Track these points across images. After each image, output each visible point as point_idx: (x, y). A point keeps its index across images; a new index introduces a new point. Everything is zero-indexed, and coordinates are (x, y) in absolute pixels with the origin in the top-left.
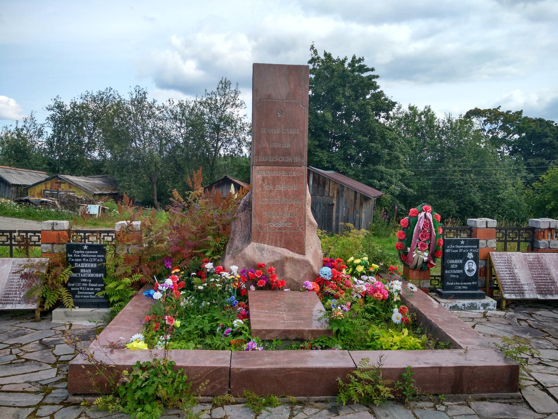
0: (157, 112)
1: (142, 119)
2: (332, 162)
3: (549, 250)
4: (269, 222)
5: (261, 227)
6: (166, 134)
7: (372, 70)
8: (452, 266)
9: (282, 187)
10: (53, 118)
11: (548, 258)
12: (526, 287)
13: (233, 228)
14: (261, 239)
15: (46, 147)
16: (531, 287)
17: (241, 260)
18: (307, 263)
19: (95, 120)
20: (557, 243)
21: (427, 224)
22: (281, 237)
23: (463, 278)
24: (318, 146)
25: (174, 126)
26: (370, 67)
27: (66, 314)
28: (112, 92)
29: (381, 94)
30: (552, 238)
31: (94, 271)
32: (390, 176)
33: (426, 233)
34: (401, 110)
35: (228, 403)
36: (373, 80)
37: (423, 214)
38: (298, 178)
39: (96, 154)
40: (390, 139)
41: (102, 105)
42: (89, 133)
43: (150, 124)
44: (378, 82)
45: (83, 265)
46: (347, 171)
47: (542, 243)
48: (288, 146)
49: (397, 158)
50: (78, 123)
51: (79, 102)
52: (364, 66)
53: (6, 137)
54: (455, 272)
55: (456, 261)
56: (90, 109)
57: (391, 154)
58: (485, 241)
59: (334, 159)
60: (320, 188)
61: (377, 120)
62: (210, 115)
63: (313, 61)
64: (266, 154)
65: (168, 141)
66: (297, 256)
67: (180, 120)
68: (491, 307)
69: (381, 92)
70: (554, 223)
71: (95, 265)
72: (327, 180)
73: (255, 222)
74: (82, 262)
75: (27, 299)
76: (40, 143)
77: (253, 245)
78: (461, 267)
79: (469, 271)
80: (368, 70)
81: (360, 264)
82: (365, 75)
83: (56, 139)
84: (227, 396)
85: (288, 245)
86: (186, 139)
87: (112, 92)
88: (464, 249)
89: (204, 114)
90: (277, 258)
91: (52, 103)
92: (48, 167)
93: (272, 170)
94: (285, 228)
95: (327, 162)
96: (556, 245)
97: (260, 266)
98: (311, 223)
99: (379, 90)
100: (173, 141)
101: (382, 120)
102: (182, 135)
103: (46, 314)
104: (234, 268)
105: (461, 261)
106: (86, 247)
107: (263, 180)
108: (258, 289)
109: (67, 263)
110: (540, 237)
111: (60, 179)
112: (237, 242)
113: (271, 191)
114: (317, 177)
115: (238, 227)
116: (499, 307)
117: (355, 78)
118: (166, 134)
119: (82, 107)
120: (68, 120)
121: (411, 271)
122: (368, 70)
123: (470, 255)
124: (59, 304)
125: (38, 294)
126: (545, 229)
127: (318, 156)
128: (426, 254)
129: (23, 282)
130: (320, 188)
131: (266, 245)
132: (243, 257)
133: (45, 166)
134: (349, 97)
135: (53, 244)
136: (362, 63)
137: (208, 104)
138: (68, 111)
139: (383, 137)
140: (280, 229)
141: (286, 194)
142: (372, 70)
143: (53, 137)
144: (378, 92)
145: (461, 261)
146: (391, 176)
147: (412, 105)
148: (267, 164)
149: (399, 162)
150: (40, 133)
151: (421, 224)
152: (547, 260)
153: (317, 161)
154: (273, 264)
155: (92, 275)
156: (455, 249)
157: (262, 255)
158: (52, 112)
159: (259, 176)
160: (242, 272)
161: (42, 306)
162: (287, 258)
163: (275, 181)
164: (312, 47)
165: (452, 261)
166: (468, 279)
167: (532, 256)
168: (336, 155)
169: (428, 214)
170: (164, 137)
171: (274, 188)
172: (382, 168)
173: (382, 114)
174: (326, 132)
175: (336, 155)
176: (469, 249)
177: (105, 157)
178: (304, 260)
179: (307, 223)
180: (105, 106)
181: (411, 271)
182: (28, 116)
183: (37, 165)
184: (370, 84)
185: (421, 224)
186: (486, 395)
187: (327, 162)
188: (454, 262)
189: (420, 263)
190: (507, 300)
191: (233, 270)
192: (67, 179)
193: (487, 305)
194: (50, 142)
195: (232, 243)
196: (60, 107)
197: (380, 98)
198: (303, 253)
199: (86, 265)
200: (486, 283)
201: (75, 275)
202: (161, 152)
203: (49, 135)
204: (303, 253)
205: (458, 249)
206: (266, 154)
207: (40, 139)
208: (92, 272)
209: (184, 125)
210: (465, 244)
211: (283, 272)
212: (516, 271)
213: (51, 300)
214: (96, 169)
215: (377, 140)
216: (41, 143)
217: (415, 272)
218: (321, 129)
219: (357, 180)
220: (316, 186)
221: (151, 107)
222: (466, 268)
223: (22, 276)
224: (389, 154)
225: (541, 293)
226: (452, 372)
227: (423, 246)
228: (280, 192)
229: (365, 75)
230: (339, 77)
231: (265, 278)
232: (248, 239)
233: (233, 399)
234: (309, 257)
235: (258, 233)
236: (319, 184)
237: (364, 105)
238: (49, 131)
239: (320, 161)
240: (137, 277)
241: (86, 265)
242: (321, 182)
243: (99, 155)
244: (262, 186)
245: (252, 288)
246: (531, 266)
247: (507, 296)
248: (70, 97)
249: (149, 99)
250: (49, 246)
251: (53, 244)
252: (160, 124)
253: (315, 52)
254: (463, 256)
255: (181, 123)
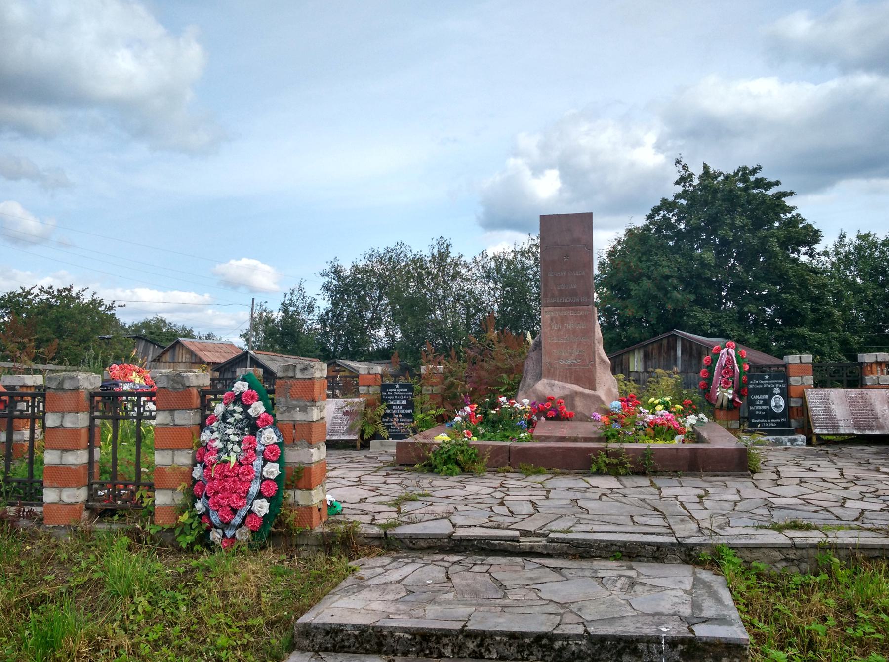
0: (463, 271)
1: (444, 281)
2: (720, 326)
3: (877, 385)
4: (559, 359)
5: (551, 364)
6: (476, 300)
7: (777, 183)
8: (757, 402)
9: (570, 326)
10: (327, 288)
11: (875, 396)
12: (841, 423)
13: (525, 367)
14: (551, 375)
15: (319, 326)
16: (848, 423)
17: (532, 395)
18: (598, 399)
19: (381, 287)
20: (885, 378)
21: (729, 361)
22: (571, 374)
23: (770, 414)
24: (696, 302)
25: (487, 288)
26: (773, 180)
27: (382, 445)
28: (403, 248)
29: (796, 220)
30: (882, 373)
31: (404, 407)
32: (818, 342)
33: (728, 369)
34: (847, 241)
35: (508, 472)
36: (783, 199)
37: (725, 350)
38: (586, 316)
39: (381, 333)
40: (815, 287)
41: (389, 267)
42: (374, 305)
43: (455, 286)
44: (789, 202)
45: (395, 402)
46: (746, 337)
47: (869, 379)
48: (575, 287)
49: (830, 315)
50: (359, 292)
51: (361, 264)
52: (762, 180)
53: (261, 318)
54: (760, 408)
55: (761, 397)
56: (375, 273)
57: (819, 309)
58: (799, 378)
59: (722, 321)
60: (694, 362)
61: (795, 260)
62: (535, 269)
63: (682, 180)
64: (553, 296)
65: (478, 310)
66: (587, 391)
67: (494, 279)
68: (799, 443)
69: (798, 215)
70: (882, 356)
71: (405, 402)
72: (703, 349)
73: (545, 360)
74: (395, 399)
75: (350, 431)
76: (310, 322)
77: (544, 381)
78: (767, 402)
79: (776, 406)
80: (769, 185)
81: (659, 403)
82: (771, 192)
83: (330, 315)
84: (507, 467)
85: (577, 382)
86: (502, 306)
87: (403, 248)
88: (769, 384)
89: (528, 268)
90: (567, 393)
91: (328, 268)
92: (321, 354)
93: (560, 310)
94: (575, 365)
95: (712, 326)
96: (886, 381)
97: (551, 399)
98: (603, 361)
99: (794, 213)
100: (484, 310)
101: (804, 259)
102: (497, 298)
103: (365, 445)
104: (526, 401)
105: (767, 397)
106: (397, 386)
107: (552, 320)
108: (547, 419)
109: (383, 400)
110: (867, 373)
111: (339, 366)
112: (529, 380)
113: (559, 330)
114: (688, 345)
115: (530, 366)
116: (809, 442)
117: (751, 199)
118: (476, 300)
119: (364, 271)
120: (347, 288)
121: (717, 411)
122: (769, 185)
123: (777, 390)
124: (376, 436)
125: (358, 427)
126: (871, 363)
127: (695, 317)
128: (731, 392)
129: (345, 418)
130: (694, 362)
131: (556, 382)
132: (535, 392)
133: (318, 352)
134: (742, 228)
135: (369, 386)
136: (758, 175)
137: (533, 253)
138: (348, 277)
139: (803, 284)
140: (569, 366)
141: (574, 332)
142: (777, 183)
143: (327, 314)
144: (793, 216)
145: (767, 397)
146: (822, 344)
147: (862, 233)
148: (554, 304)
149: (833, 322)
150: (310, 308)
151: (723, 359)
152: (873, 397)
153: (693, 325)
154: (563, 398)
155: (403, 411)
156: (758, 384)
157: (552, 390)
158: (326, 280)
159: (548, 317)
160: (533, 404)
161: (361, 437)
162: (576, 393)
163: (564, 320)
164: (678, 162)
165: (757, 397)
166: (775, 416)
167: (853, 392)
168: (727, 315)
169: (730, 350)
170: (474, 304)
171: (563, 326)
172: (805, 331)
173: (803, 250)
174: (708, 280)
175: (727, 315)
176: (774, 383)
177: (393, 337)
178: (594, 396)
179: (597, 360)
180: (394, 268)
181: (717, 411)
182: (295, 285)
183: (308, 351)
184: (777, 205)
185: (723, 359)
186: (719, 473)
187: (712, 326)
188: (759, 398)
189: (725, 403)
190: (818, 436)
191: (524, 403)
192: (348, 366)
193: (795, 440)
194: (323, 320)
195: (525, 381)
196: (337, 272)
197: (796, 226)
198: (594, 389)
199: (398, 402)
200: (796, 421)
201: (388, 411)
202: (468, 325)
203: (322, 310)
204: (594, 389)
205: (762, 384)
206: (553, 296)
207: (310, 317)
208: (403, 408)
209: (499, 285)
210: (770, 379)
211: (573, 406)
212: (833, 407)
213: (370, 431)
214: (383, 355)
215: (793, 289)
216: (311, 321)
217: (722, 413)
218: (699, 277)
219: (763, 352)
220: (687, 358)
221: (456, 265)
222: (773, 404)
223: (344, 414)
224: (814, 310)
225: (858, 429)
226: (688, 453)
227: (726, 383)
228: (568, 330)
229: (771, 192)
230: (723, 200)
231: (553, 409)
232: (539, 377)
233: (513, 470)
234: (601, 393)
235: (549, 370)
236: (691, 355)
237: (766, 237)
238: (323, 304)
239: (699, 325)
240: (441, 411)
241: (398, 402)
242: (695, 353)
243: (386, 334)
244: (551, 327)
245: (543, 418)
246: (852, 402)
247: (817, 431)
248: (351, 257)
249: (454, 254)
250: (366, 388)
251: (369, 386)
252: (468, 286)
253: (685, 168)
254: (769, 392)
255: (496, 283)
